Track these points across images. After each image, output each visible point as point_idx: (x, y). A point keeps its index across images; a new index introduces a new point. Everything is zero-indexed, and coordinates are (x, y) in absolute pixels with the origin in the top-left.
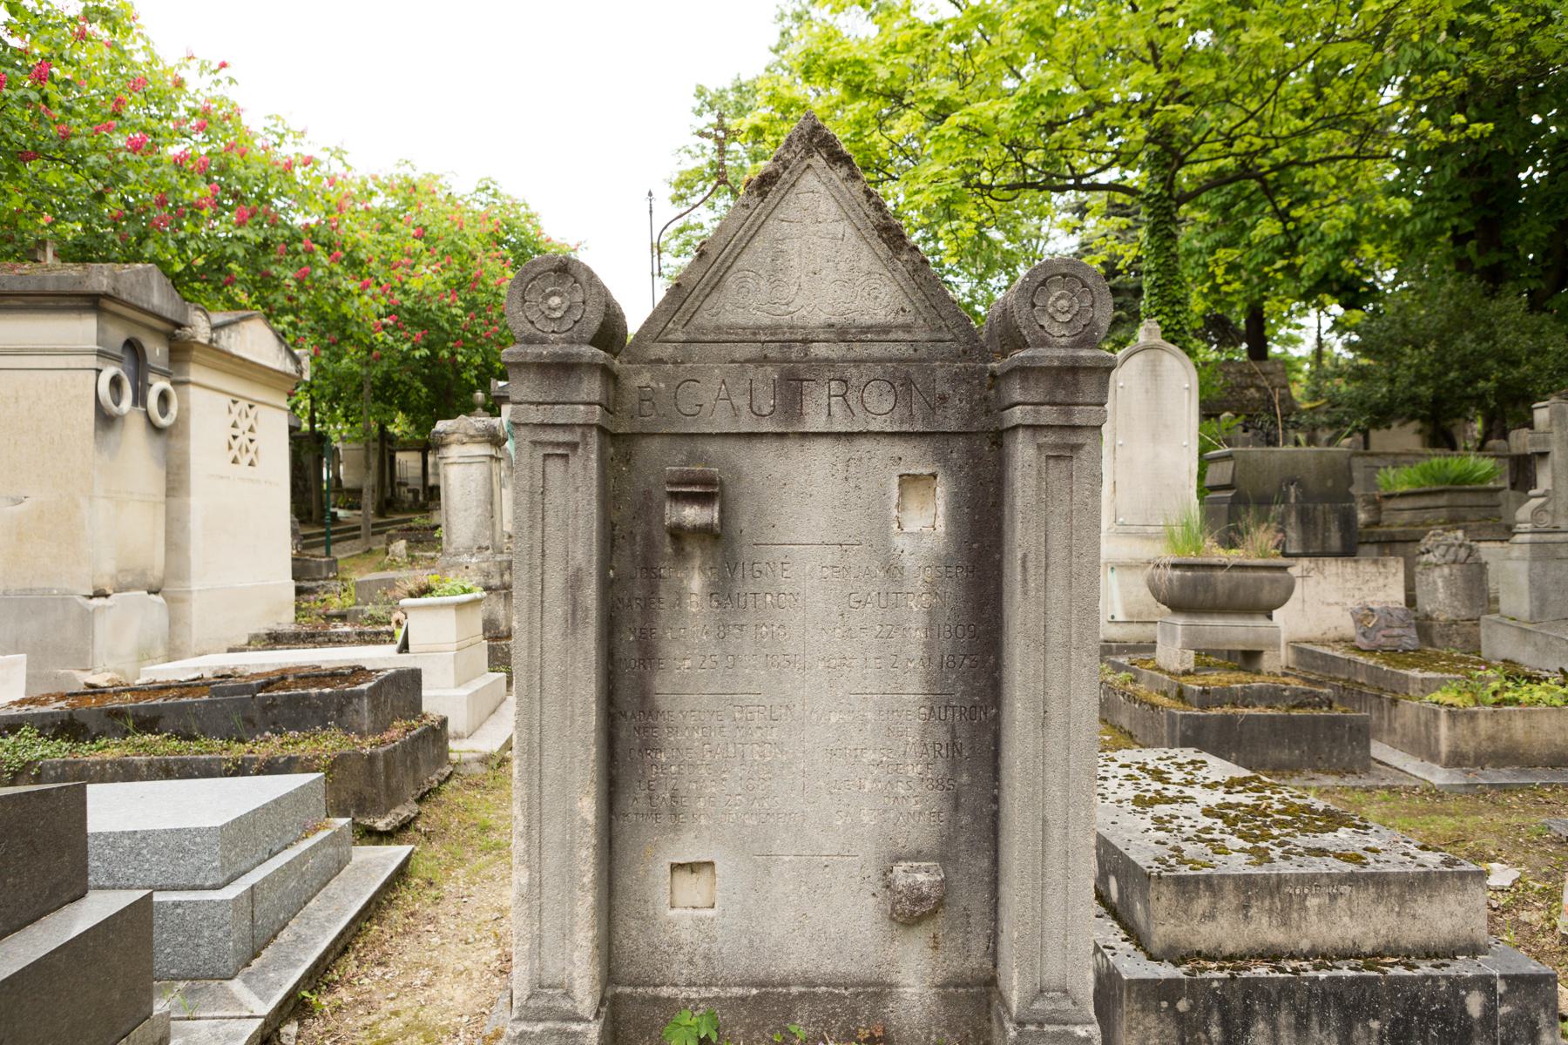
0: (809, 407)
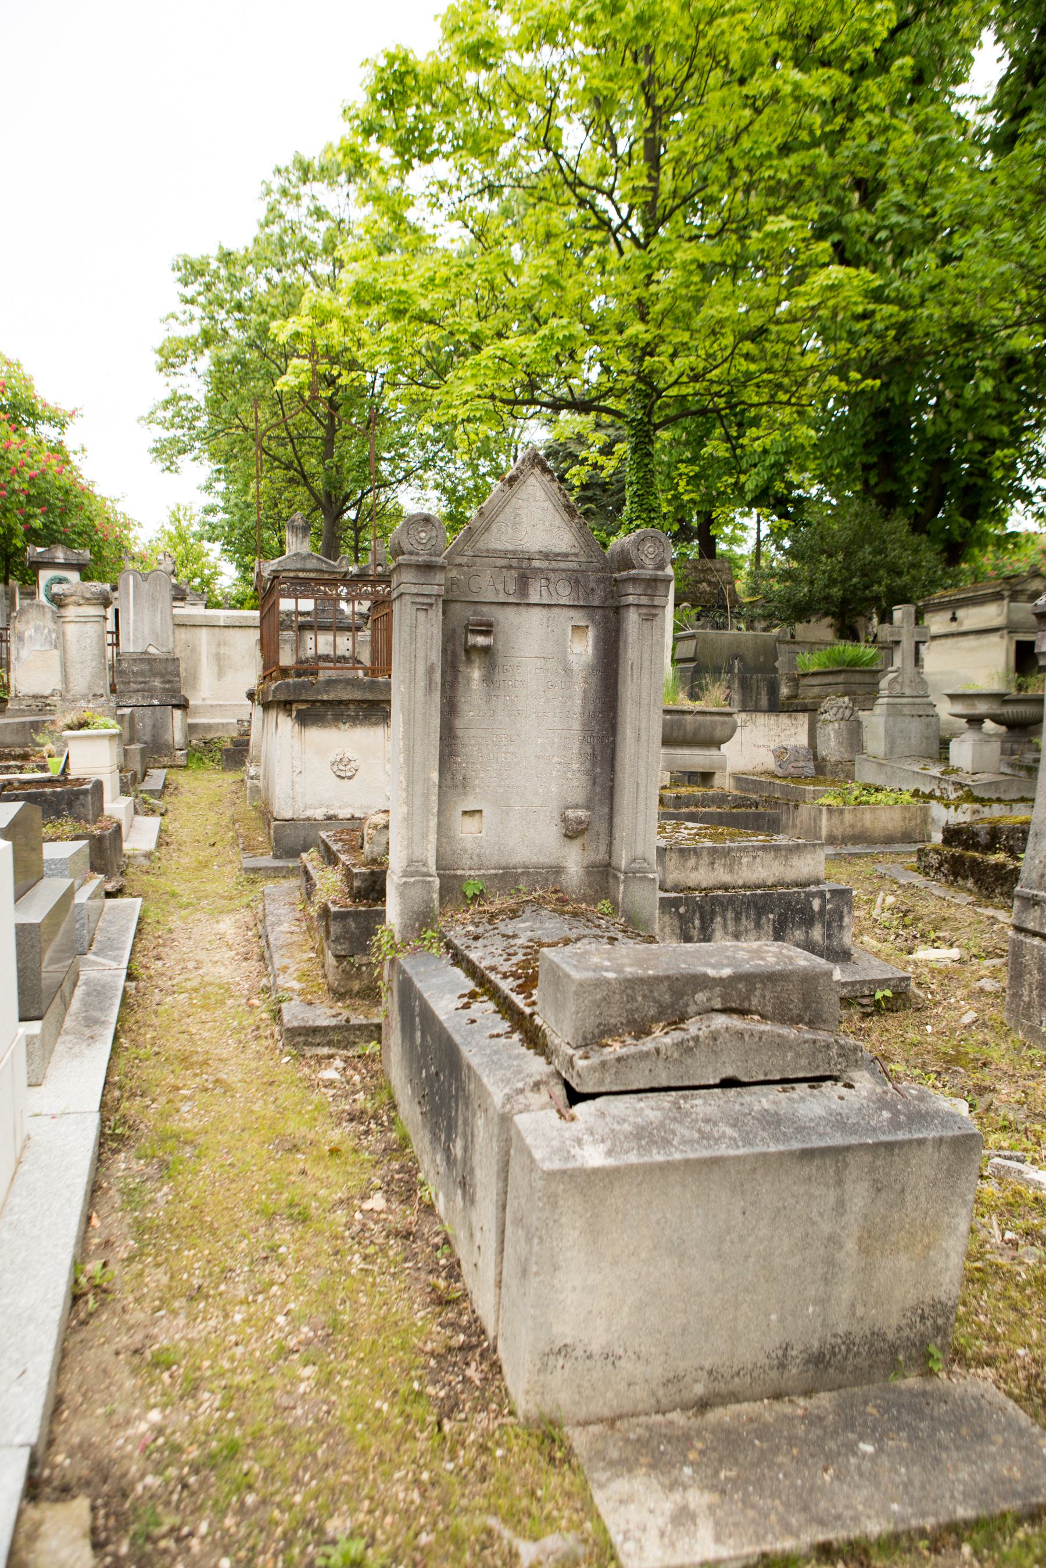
0: (531, 591)
